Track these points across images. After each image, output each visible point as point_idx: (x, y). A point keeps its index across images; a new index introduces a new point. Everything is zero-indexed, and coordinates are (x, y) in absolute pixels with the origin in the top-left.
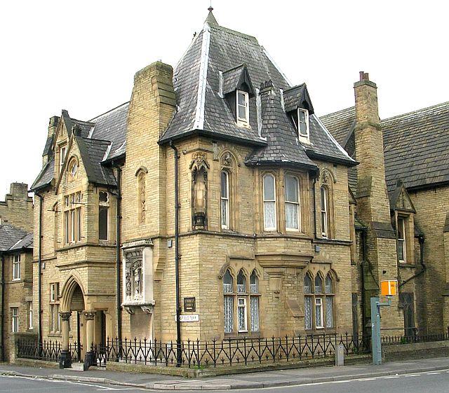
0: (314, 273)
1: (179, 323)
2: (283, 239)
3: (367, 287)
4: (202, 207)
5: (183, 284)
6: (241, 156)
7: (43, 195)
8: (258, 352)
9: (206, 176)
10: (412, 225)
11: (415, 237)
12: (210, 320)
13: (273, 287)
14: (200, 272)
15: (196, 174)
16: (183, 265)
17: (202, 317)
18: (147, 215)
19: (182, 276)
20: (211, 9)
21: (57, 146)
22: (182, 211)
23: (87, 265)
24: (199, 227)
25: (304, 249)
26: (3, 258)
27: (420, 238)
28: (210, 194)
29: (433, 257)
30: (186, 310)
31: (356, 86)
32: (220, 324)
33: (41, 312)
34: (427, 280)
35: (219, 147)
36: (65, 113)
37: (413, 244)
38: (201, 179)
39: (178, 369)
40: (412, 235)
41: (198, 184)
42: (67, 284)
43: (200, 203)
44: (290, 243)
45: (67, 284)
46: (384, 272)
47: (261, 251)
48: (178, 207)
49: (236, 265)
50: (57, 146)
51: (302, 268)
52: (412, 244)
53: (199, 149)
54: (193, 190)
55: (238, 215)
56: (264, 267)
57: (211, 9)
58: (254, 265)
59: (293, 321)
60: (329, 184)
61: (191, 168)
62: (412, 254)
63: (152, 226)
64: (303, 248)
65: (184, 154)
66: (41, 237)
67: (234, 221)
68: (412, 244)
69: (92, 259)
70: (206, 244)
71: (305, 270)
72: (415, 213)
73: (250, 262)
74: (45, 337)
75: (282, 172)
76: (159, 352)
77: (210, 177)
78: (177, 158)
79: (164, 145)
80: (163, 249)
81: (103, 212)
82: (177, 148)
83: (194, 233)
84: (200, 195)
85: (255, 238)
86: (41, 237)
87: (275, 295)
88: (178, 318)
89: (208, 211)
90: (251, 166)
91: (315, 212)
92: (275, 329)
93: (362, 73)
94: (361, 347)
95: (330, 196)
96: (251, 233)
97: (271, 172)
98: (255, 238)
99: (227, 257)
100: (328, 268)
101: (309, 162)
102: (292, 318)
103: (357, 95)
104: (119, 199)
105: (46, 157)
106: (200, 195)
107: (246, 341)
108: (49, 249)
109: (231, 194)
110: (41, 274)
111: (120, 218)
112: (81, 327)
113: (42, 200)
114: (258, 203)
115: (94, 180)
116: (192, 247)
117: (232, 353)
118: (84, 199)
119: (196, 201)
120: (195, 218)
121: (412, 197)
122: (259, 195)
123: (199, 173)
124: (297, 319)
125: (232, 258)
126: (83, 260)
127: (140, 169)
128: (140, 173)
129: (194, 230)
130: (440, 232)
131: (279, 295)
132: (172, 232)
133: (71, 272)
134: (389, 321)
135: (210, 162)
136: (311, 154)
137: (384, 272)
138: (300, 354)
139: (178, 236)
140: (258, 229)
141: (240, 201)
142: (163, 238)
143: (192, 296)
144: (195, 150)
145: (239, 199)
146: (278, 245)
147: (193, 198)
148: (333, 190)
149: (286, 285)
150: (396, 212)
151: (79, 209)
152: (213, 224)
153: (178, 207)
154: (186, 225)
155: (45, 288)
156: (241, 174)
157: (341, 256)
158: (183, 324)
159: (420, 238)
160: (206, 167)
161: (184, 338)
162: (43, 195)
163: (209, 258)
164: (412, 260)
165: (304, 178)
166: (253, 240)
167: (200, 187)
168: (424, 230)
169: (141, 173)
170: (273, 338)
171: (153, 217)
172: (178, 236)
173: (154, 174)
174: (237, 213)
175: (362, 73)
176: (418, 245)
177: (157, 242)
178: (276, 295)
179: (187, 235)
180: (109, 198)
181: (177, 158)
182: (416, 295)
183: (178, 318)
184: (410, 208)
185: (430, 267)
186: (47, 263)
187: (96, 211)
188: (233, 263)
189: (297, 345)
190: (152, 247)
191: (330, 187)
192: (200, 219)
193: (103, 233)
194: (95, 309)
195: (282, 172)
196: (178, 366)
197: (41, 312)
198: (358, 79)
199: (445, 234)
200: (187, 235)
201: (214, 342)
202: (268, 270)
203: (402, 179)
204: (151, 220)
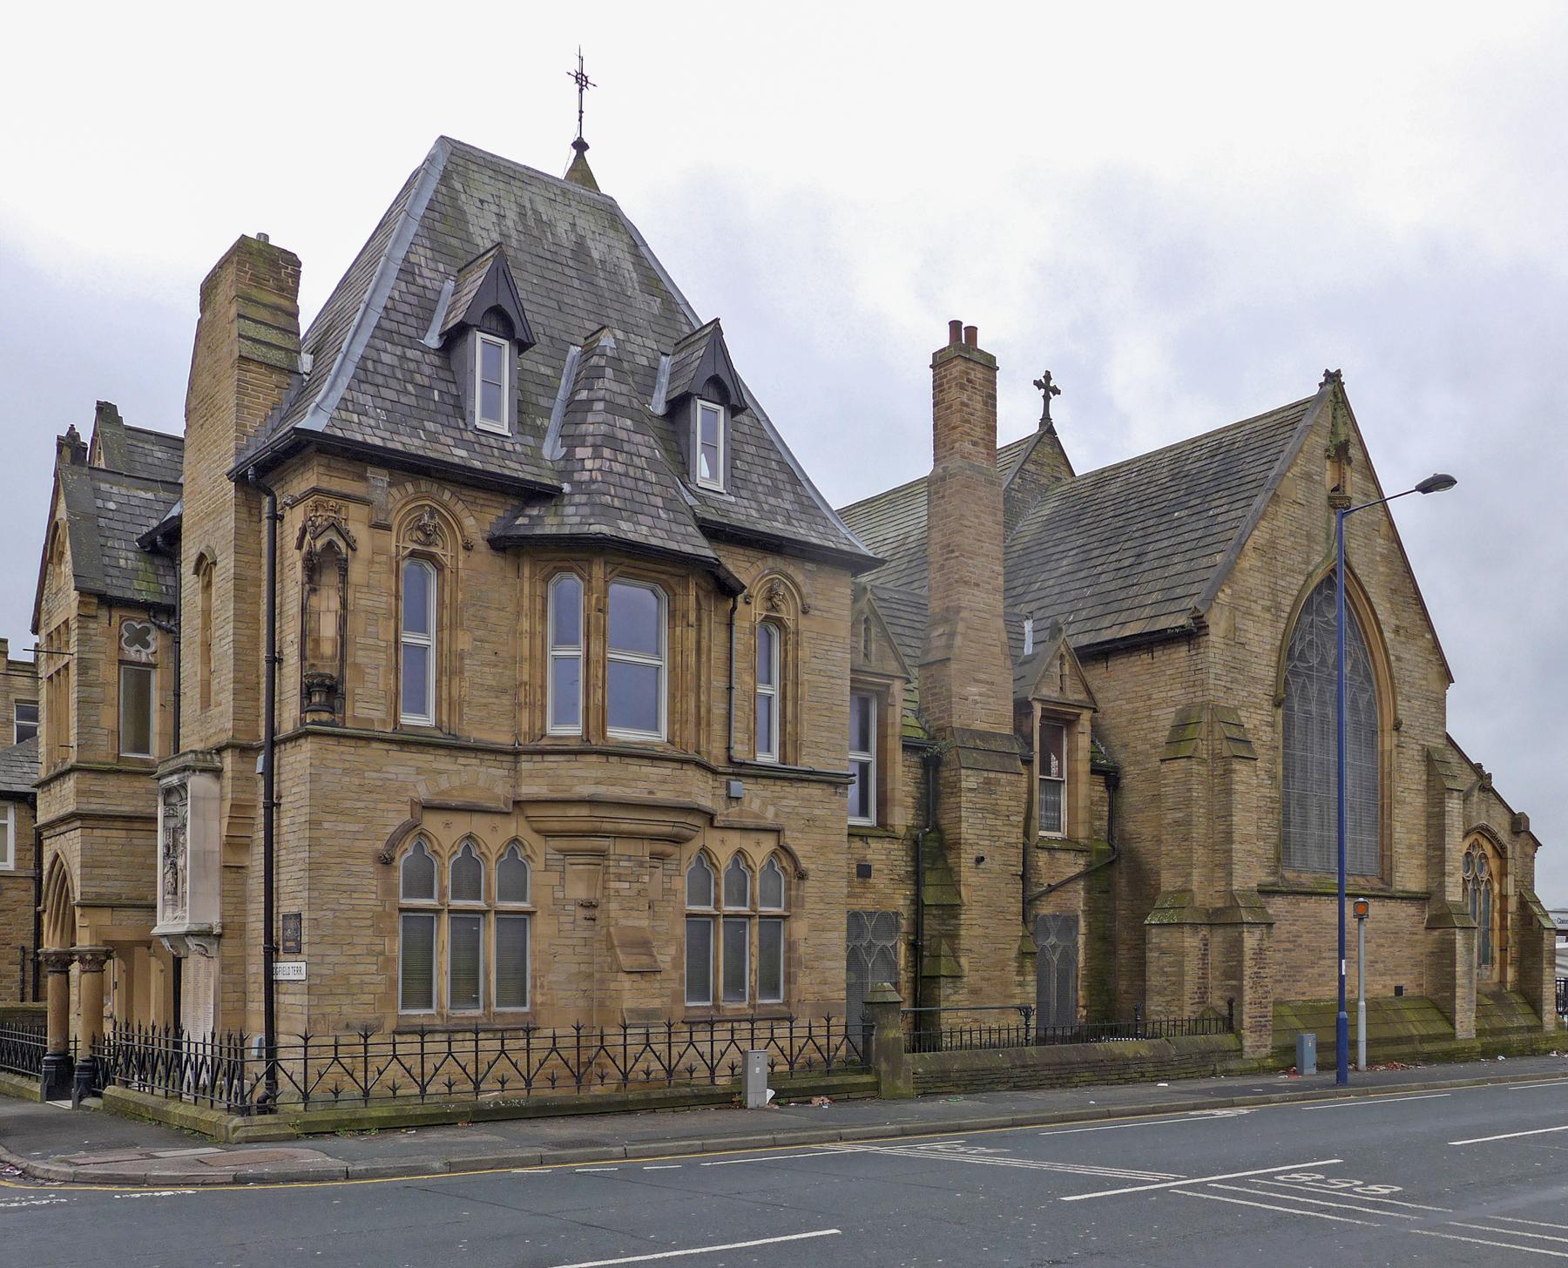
0: (724, 857)
2: (594, 758)
3: (930, 896)
6: (478, 519)
8: (359, 1075)
10: (1084, 741)
11: (1093, 772)
12: (346, 978)
13: (579, 891)
14: (313, 842)
15: (313, 568)
17: (315, 969)
20: (580, 146)
23: (78, 823)
24: (316, 717)
25: (665, 787)
27: (1109, 776)
28: (356, 624)
29: (1139, 827)
31: (940, 361)
32: (382, 989)
34: (1122, 884)
35: (394, 491)
36: (106, 412)
37: (1088, 790)
41: (324, 592)
43: (327, 649)
44: (615, 767)
46: (980, 860)
47: (529, 790)
49: (495, 829)
52: (1083, 789)
53: (315, 491)
54: (303, 609)
56: (548, 834)
57: (580, 146)
58: (513, 827)
59: (626, 982)
60: (787, 613)
61: (299, 547)
62: (1082, 815)
68: (1083, 789)
69: (94, 806)
70: (339, 765)
71: (693, 848)
73: (497, 820)
77: (357, 572)
81: (138, 677)
84: (328, 628)
85: (516, 754)
89: (348, 673)
90: (505, 545)
91: (730, 688)
92: (582, 1003)
93: (955, 326)
94: (894, 1046)
95: (790, 648)
96: (503, 739)
98: (516, 754)
99: (413, 803)
100: (769, 843)
101: (701, 547)
102: (622, 976)
106: (328, 628)
107: (481, 1036)
114: (526, 653)
115: (98, 586)
116: (296, 761)
117: (796, 1050)
119: (317, 642)
120: (307, 692)
122: (532, 635)
123: (324, 564)
124: (634, 977)
125: (429, 807)
129: (303, 722)
131: (597, 913)
134: (989, 991)
135: (358, 529)
136: (714, 532)
140: (525, 727)
141: (467, 647)
142: (244, 751)
145: (464, 642)
146: (577, 773)
148: (797, 633)
149: (612, 885)
151: (66, 666)
152: (366, 704)
154: (289, 715)
156: (480, 572)
157: (816, 812)
158: (283, 988)
159: (1109, 776)
160: (342, 544)
163: (348, 804)
164: (1082, 833)
165: (679, 590)
166: (510, 758)
167: (327, 601)
168: (1122, 757)
170: (578, 1029)
172: (273, 744)
173: (226, 565)
174: (456, 681)
175: (955, 326)
176: (1100, 790)
177: (228, 761)
178: (587, 913)
185: (1131, 851)
188: (432, 823)
190: (218, 773)
191: (790, 624)
192: (325, 691)
194: (106, 942)
195: (598, 571)
198: (944, 341)
199: (1164, 767)
201: (366, 1038)
203: (1061, 619)
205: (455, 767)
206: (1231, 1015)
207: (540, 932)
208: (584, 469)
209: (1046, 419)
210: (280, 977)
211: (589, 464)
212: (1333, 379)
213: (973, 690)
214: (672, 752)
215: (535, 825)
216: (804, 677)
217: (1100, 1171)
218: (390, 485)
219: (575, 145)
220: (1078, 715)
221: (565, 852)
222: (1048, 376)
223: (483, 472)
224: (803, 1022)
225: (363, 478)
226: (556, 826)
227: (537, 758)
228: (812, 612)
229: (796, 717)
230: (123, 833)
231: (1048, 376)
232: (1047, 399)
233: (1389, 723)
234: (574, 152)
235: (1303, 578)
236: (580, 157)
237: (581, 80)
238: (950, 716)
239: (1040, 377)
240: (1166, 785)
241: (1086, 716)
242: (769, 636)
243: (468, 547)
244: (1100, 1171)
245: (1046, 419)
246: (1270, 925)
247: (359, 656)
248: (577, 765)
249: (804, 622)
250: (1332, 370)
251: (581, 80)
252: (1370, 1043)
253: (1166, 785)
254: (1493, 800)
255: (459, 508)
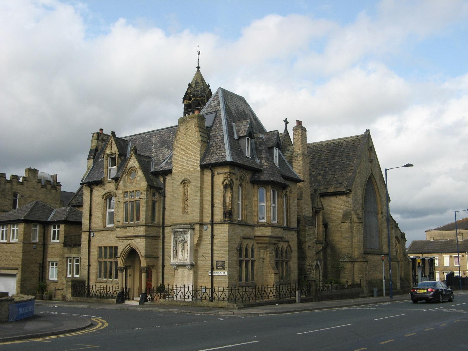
0: (280, 247)
1: (212, 276)
4: (229, 207)
5: (215, 253)
6: (248, 176)
7: (92, 187)
9: (232, 189)
10: (321, 217)
15: (226, 187)
16: (216, 241)
18: (190, 209)
19: (215, 248)
20: (198, 68)
21: (106, 156)
22: (215, 208)
26: (44, 226)
27: (326, 225)
30: (217, 268)
33: (89, 266)
37: (322, 228)
38: (229, 190)
39: (212, 303)
40: (321, 223)
42: (127, 248)
43: (227, 205)
45: (127, 248)
46: (309, 246)
48: (213, 206)
50: (106, 156)
51: (275, 244)
55: (245, 212)
56: (258, 243)
57: (198, 68)
61: (223, 183)
63: (194, 216)
64: (279, 232)
65: (218, 174)
66: (91, 215)
67: (244, 216)
72: (323, 210)
74: (92, 283)
75: (270, 187)
76: (114, 293)
77: (234, 189)
78: (213, 176)
79: (203, 167)
80: (201, 231)
82: (213, 170)
83: (224, 222)
84: (228, 200)
86: (91, 215)
87: (262, 260)
88: (212, 273)
97: (263, 187)
103: (285, 131)
104: (164, 197)
105: (91, 161)
106: (228, 200)
108: (97, 223)
109: (242, 199)
110: (90, 240)
111: (164, 208)
112: (128, 277)
113: (92, 191)
118: (143, 196)
120: (225, 214)
121: (322, 199)
125: (244, 238)
126: (141, 234)
127: (185, 180)
128: (132, 169)
130: (338, 222)
132: (207, 219)
133: (129, 242)
137: (309, 246)
138: (219, 298)
139: (212, 223)
141: (247, 203)
143: (222, 260)
144: (226, 173)
147: (224, 202)
148: (290, 197)
150: (314, 209)
153: (213, 206)
154: (219, 216)
155: (92, 249)
156: (247, 186)
158: (214, 277)
159: (326, 225)
160: (232, 183)
161: (215, 286)
162: (92, 187)
169: (185, 182)
171: (194, 211)
173: (193, 188)
179: (219, 224)
180: (157, 195)
181: (213, 176)
182: (171, 246)
183: (212, 273)
184: (321, 206)
186: (96, 233)
187: (150, 203)
189: (100, 290)
190: (193, 229)
191: (288, 195)
192: (228, 215)
193: (153, 219)
196: (212, 301)
197: (89, 266)
199: (342, 224)
200: (219, 224)
202: (259, 245)
204: (193, 212)
205: (245, 229)
206: (361, 283)
207: (256, 264)
208: (264, 165)
209: (286, 130)
210: (214, 275)
211: (265, 164)
212: (368, 131)
213: (306, 206)
214: (278, 225)
215: (257, 242)
216: (291, 207)
217: (43, 341)
218: (238, 170)
219: (197, 68)
220: (320, 211)
221: (260, 247)
222: (286, 119)
223: (257, 169)
224: (292, 285)
225: (234, 169)
226: (261, 242)
227: (259, 227)
228: (292, 192)
229: (290, 216)
230: (151, 240)
231: (286, 119)
232: (286, 125)
233: (380, 212)
234: (197, 69)
235: (365, 178)
236: (198, 70)
237: (199, 52)
238: (302, 213)
239: (285, 119)
240: (343, 228)
241: (322, 211)
242: (239, 188)
243: (247, 183)
244: (43, 341)
245: (286, 130)
246: (367, 262)
247: (235, 207)
248: (266, 229)
249: (291, 195)
250: (368, 129)
251: (199, 52)
252: (386, 290)
253: (343, 228)
254: (398, 230)
255: (246, 174)
